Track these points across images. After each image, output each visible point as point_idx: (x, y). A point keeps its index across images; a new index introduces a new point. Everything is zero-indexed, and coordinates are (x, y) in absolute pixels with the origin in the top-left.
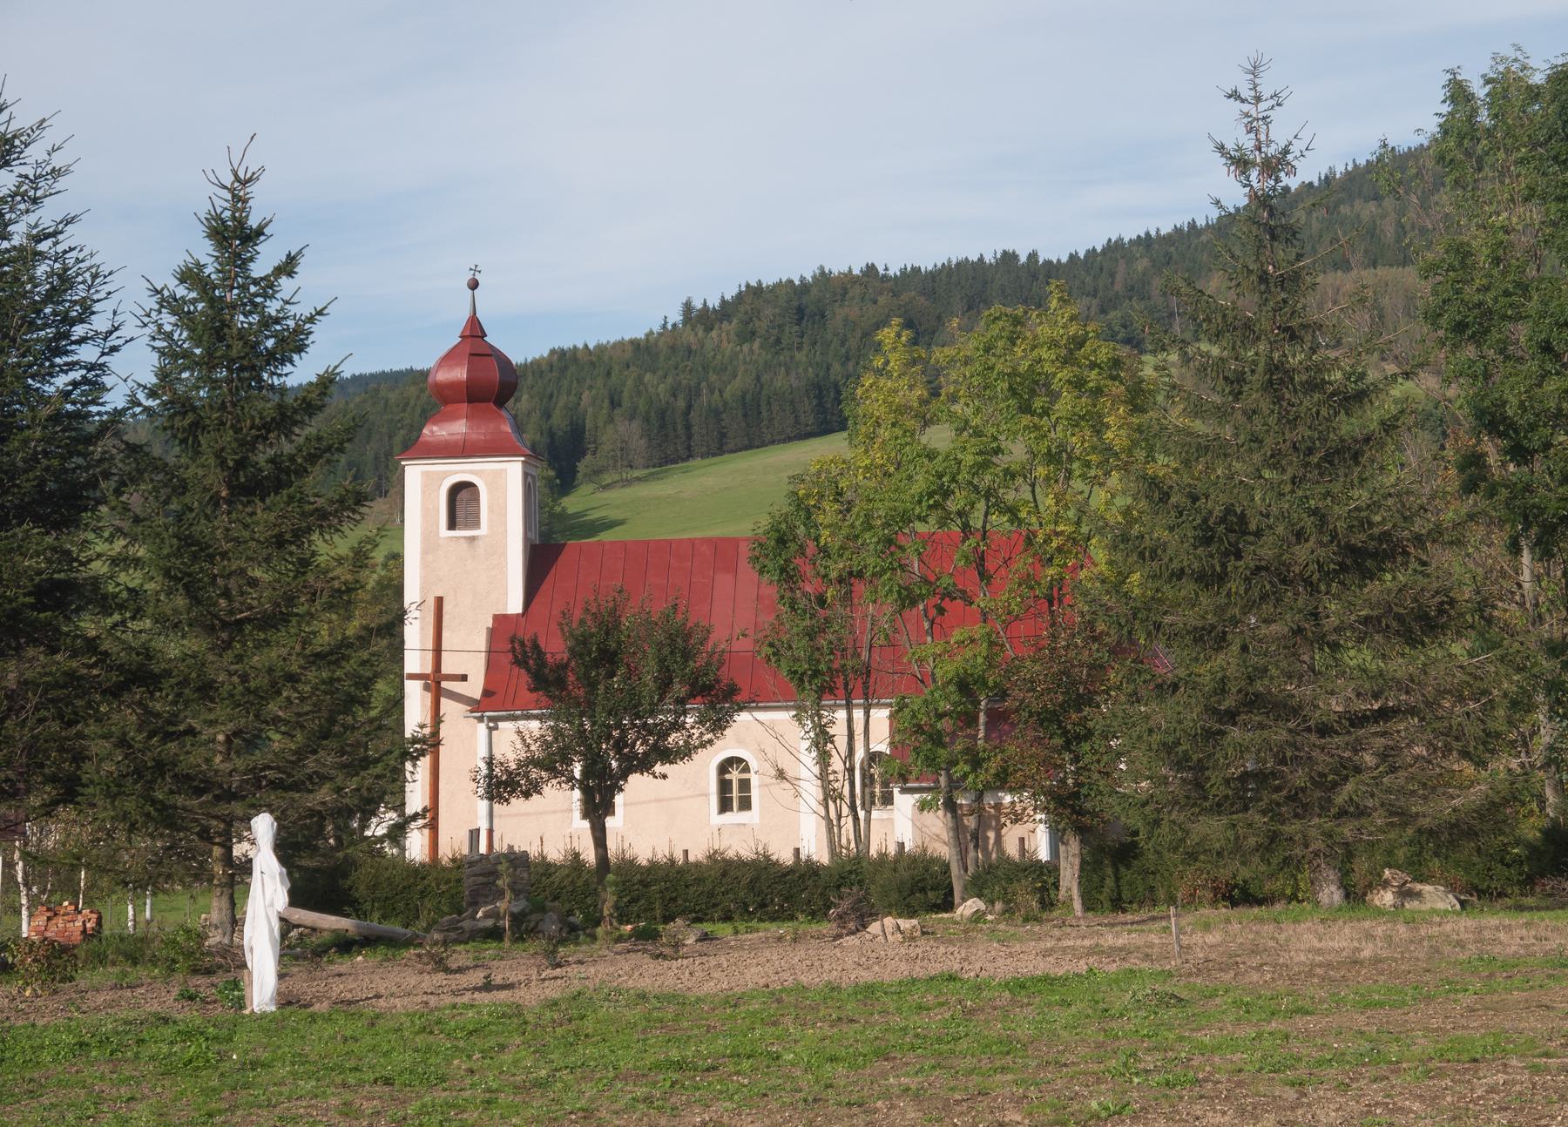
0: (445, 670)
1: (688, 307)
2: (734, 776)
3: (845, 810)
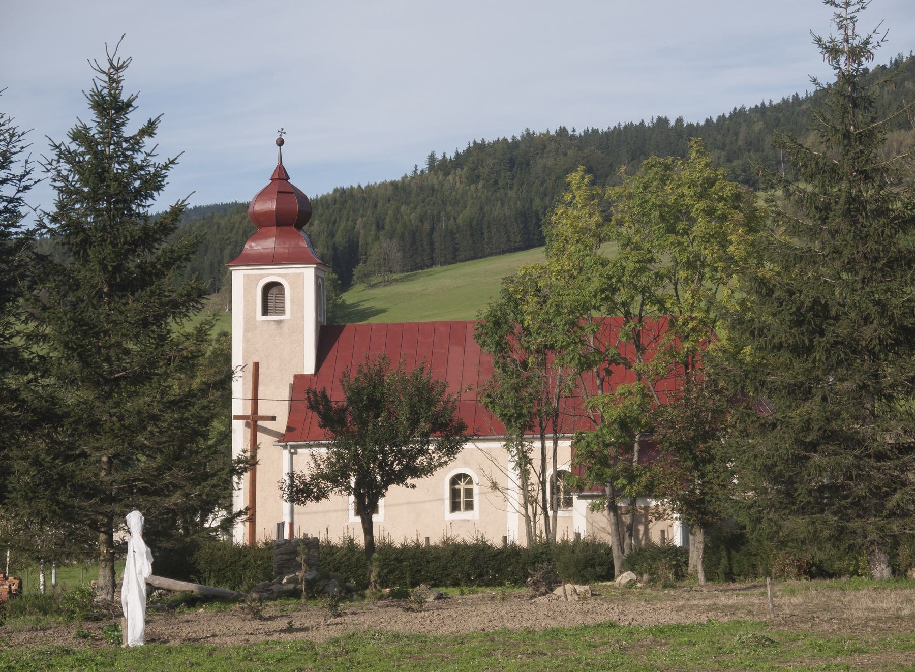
1: (432, 158)
2: (462, 486)
3: (539, 510)
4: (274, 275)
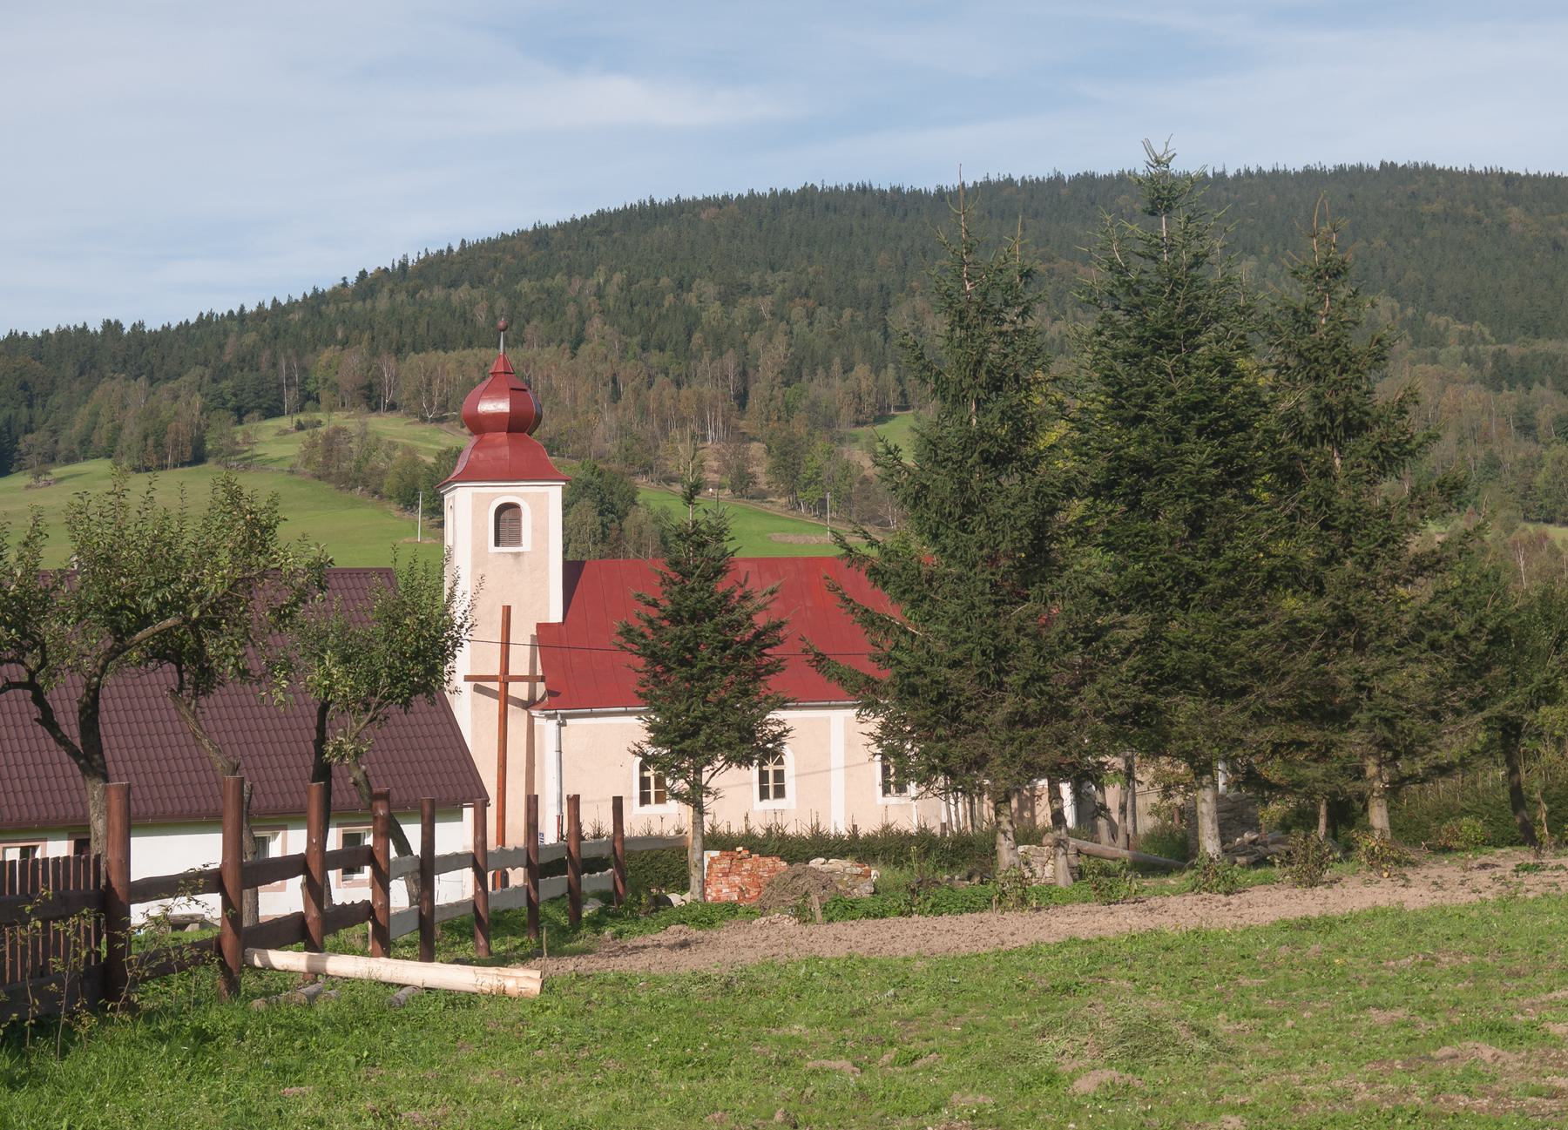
0: (511, 673)
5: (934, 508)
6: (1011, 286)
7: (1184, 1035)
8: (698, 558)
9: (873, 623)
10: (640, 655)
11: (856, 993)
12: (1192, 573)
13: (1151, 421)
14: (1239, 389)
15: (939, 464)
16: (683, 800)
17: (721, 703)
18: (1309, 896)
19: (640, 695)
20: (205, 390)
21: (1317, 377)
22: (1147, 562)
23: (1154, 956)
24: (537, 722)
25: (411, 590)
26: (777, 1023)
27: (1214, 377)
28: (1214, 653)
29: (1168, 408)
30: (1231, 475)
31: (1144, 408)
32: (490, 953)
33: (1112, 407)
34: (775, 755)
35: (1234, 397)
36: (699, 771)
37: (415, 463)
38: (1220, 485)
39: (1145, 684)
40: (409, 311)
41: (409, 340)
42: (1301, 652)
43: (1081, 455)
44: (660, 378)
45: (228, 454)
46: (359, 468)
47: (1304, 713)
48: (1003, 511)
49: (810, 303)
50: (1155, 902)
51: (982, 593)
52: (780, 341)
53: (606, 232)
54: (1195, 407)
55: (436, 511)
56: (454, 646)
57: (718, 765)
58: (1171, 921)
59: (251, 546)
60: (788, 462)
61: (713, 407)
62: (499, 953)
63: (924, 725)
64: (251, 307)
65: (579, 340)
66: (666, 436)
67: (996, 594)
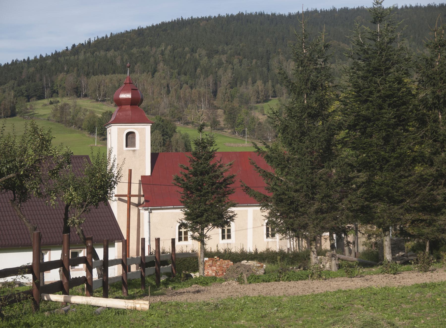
0: (137, 194)
4: (131, 128)
5: (290, 134)
6: (320, 51)
7: (385, 325)
8: (204, 152)
9: (267, 176)
10: (182, 187)
11: (263, 309)
12: (385, 158)
13: (371, 101)
14: (405, 89)
15: (292, 117)
16: (197, 240)
17: (212, 204)
18: (425, 275)
19: (182, 202)
20: (15, 89)
21: (434, 85)
22: (368, 154)
23: (370, 295)
24: (141, 211)
25: (98, 163)
26: (235, 320)
27: (396, 86)
28: (392, 187)
29: (377, 97)
30: (400, 121)
31: (368, 97)
32: (128, 295)
33: (356, 97)
34: (228, 223)
35: (402, 92)
36: (203, 229)
37: (94, 117)
38: (396, 125)
39: (366, 198)
40: (91, 60)
41: (91, 71)
42: (424, 187)
43: (344, 114)
44: (185, 86)
45: (24, 114)
46: (73, 119)
47: (424, 209)
48: (316, 135)
49: (241, 57)
50: (368, 277)
51: (307, 165)
52: (229, 71)
53: (165, 30)
54: (388, 96)
55: (103, 136)
56: (114, 184)
57: (210, 227)
58: (374, 284)
59: (42, 147)
60: (232, 117)
61: (204, 96)
62: (131, 295)
63: (285, 213)
64: (32, 58)
65: (155, 71)
66: (187, 107)
67: (312, 165)
